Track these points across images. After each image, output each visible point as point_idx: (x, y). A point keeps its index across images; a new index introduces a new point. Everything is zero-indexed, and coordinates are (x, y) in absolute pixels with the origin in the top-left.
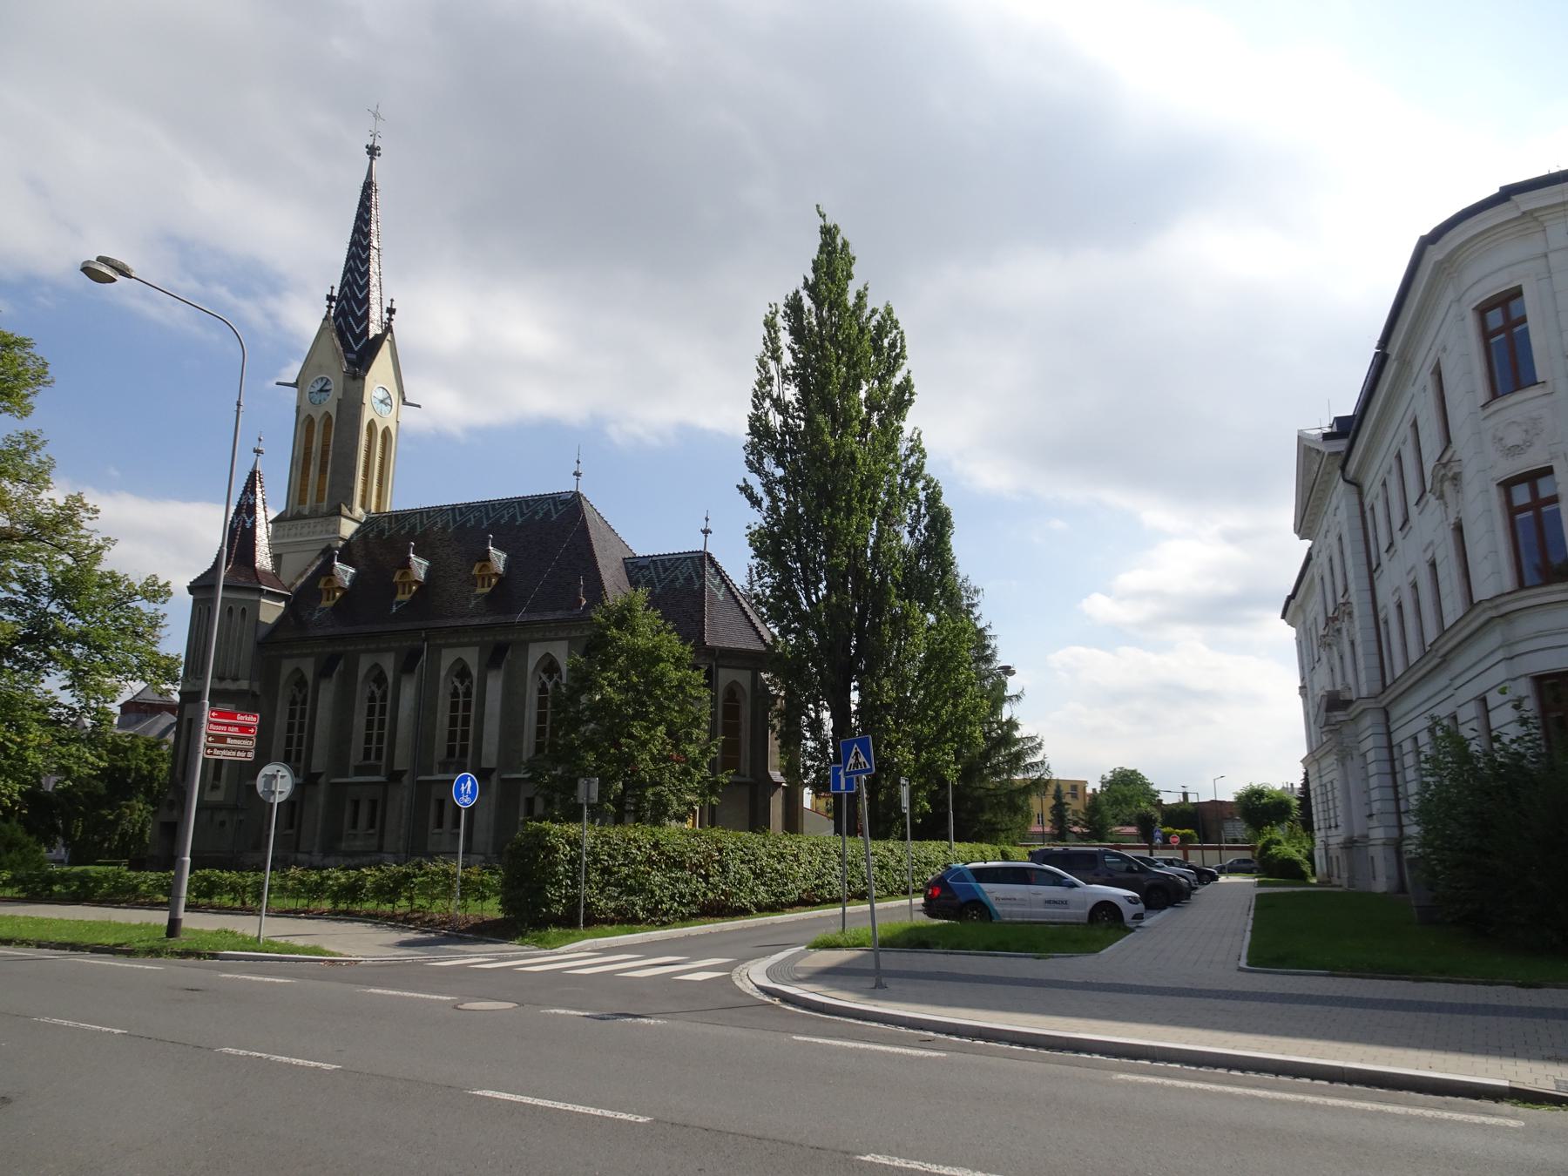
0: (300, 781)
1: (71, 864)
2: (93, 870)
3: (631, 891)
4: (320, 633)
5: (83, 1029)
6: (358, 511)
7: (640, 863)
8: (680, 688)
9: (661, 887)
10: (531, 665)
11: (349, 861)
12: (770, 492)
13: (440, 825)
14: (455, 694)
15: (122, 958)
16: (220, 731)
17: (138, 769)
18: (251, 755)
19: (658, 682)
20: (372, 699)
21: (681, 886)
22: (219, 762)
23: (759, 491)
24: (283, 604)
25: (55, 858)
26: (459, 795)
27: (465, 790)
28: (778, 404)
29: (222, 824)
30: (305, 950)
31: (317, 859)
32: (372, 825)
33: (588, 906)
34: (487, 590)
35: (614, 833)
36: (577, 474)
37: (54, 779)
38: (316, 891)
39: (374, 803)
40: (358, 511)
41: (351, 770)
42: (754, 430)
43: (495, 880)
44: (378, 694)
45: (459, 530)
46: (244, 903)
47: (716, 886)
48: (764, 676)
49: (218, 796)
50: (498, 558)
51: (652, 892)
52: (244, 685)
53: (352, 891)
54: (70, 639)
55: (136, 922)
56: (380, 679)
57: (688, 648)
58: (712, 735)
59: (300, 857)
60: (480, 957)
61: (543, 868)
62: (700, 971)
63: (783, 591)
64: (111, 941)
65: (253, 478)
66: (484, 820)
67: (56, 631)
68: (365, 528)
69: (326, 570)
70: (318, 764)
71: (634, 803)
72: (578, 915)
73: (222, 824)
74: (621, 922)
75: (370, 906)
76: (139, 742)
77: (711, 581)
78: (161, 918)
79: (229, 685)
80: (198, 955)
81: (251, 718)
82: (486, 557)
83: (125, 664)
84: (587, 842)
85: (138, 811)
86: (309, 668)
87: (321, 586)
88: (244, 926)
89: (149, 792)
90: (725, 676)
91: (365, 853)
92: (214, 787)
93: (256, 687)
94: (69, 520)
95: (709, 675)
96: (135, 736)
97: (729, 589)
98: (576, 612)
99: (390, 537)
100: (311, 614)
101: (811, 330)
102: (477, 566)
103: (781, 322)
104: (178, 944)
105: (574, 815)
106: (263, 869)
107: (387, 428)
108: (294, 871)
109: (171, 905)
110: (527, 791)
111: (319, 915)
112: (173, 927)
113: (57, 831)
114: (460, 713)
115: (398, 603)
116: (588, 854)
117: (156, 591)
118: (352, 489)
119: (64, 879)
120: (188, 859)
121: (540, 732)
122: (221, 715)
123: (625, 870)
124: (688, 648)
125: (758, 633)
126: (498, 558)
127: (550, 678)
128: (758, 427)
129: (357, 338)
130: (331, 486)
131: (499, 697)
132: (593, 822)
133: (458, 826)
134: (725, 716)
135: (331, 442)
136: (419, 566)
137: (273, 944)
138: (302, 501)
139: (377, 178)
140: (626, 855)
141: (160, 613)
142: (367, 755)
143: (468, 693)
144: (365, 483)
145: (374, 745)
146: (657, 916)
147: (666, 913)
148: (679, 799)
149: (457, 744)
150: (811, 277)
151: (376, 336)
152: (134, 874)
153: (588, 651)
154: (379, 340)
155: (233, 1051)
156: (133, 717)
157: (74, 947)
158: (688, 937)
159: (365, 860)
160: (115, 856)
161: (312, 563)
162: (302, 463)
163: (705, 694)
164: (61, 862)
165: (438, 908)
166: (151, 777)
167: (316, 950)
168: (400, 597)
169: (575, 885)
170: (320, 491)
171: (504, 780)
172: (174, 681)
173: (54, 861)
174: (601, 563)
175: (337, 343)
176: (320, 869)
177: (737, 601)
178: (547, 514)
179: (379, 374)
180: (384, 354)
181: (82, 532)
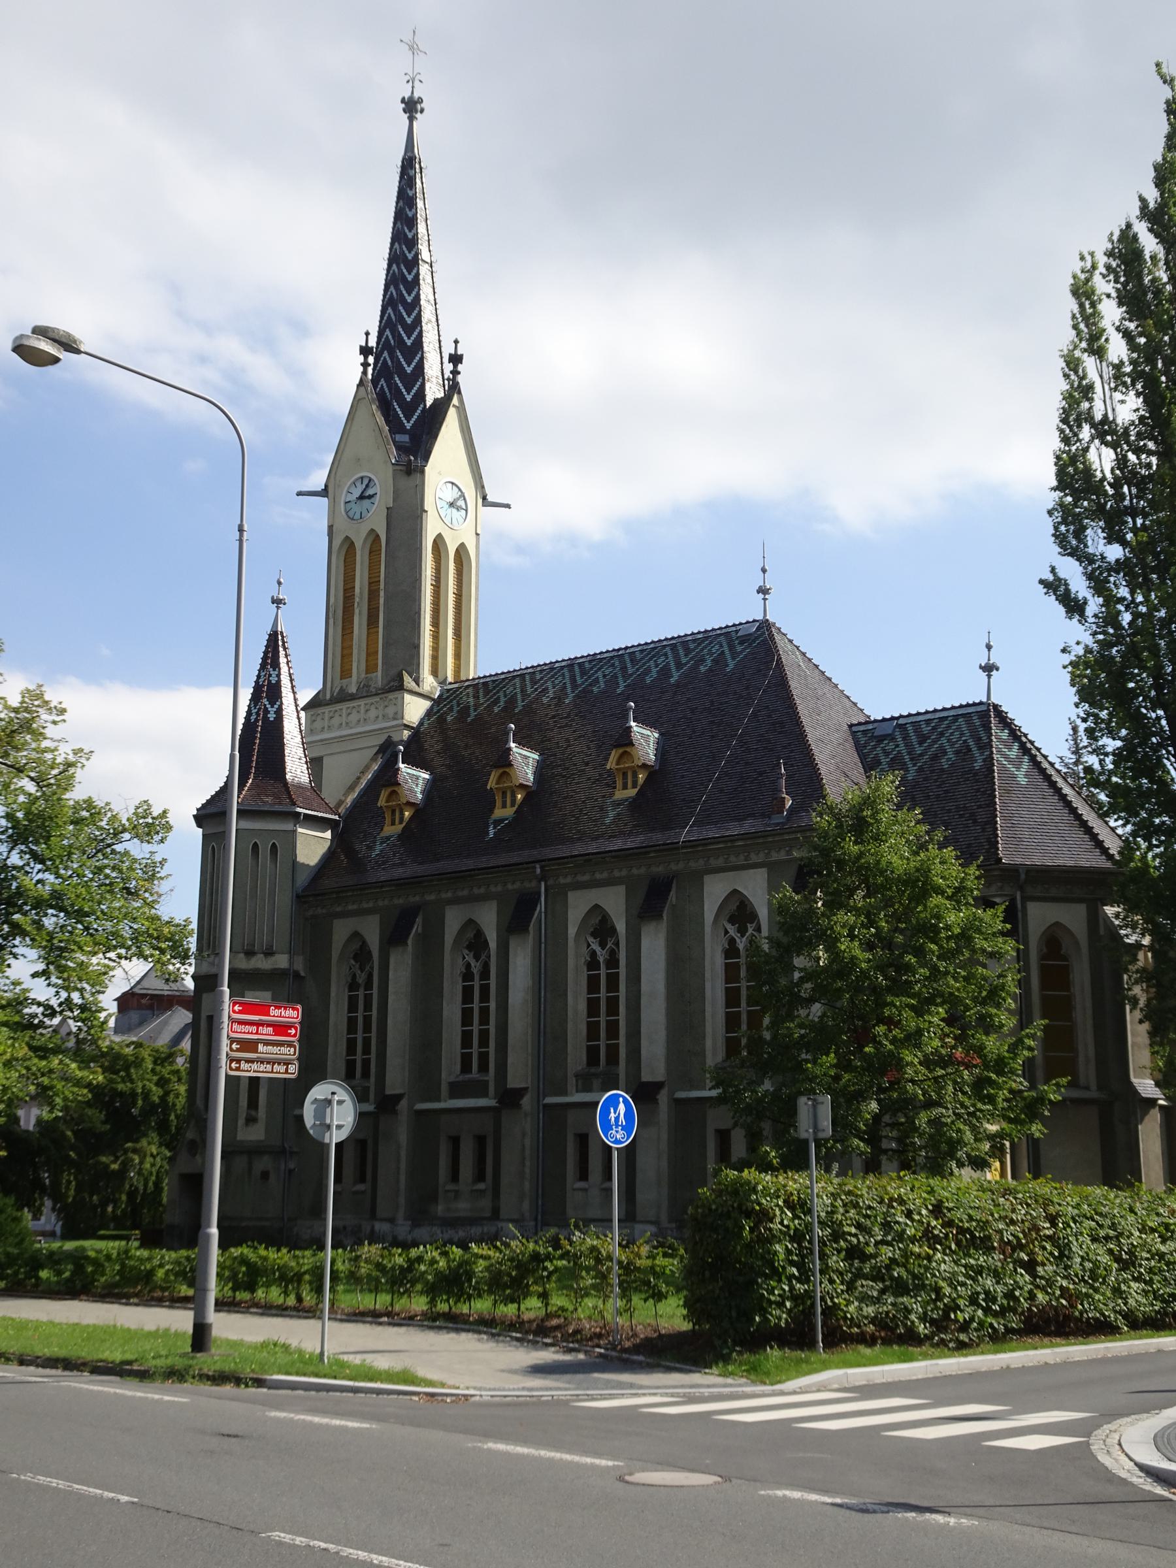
0: (369, 1107)
1: (67, 1235)
2: (92, 1246)
3: (900, 1288)
4: (383, 876)
5: (80, 1496)
6: (429, 683)
7: (913, 1240)
8: (965, 937)
9: (952, 1281)
10: (709, 914)
11: (450, 1233)
12: (1099, 585)
13: (583, 1175)
14: (593, 964)
15: (134, 1382)
16: (247, 1033)
17: (146, 1094)
18: (293, 1068)
19: (930, 931)
20: (468, 976)
21: (989, 1283)
22: (254, 1082)
23: (1079, 586)
24: (328, 834)
25: (40, 1227)
26: (607, 1127)
27: (617, 1120)
28: (1105, 430)
29: (265, 1175)
30: (390, 1377)
31: (403, 1230)
32: (480, 1176)
33: (829, 1312)
34: (632, 792)
35: (865, 1188)
36: (763, 591)
37: (35, 1112)
38: (400, 1281)
39: (481, 1140)
40: (429, 683)
41: (444, 1088)
42: (1064, 481)
43: (671, 1265)
44: (476, 967)
45: (585, 696)
46: (299, 1299)
47: (1050, 1283)
48: (1110, 910)
49: (254, 1134)
50: (646, 740)
51: (938, 1290)
52: (282, 961)
53: (454, 1283)
54: (40, 904)
55: (150, 1327)
56: (477, 944)
57: (973, 870)
58: (1024, 1018)
59: (381, 1227)
60: (658, 1394)
61: (749, 1247)
62: (1033, 1433)
63: (1139, 759)
64: (118, 1356)
65: (274, 642)
66: (652, 1166)
67: (19, 893)
68: (440, 706)
69: (387, 777)
70: (396, 1079)
71: (902, 1140)
72: (813, 1328)
73: (265, 1175)
74: (887, 1342)
75: (482, 1306)
76: (145, 1053)
77: (1003, 753)
78: (182, 1320)
79: (260, 963)
80: (238, 1381)
81: (290, 1013)
82: (625, 740)
83: (116, 934)
84: (821, 1205)
85: (150, 1156)
86: (372, 931)
87: (382, 802)
88: (300, 1334)
89: (163, 1127)
90: (1041, 915)
91: (473, 1221)
92: (251, 1120)
93: (299, 966)
94: (27, 726)
95: (1011, 915)
96: (139, 1045)
97: (1033, 759)
98: (776, 819)
99: (478, 718)
100: (370, 848)
101: (1158, 292)
102: (614, 755)
103: (1103, 286)
104: (208, 1362)
105: (795, 1160)
106: (322, 1247)
107: (462, 545)
108: (370, 1251)
109: (195, 1302)
110: (718, 1119)
111: (408, 1320)
112: (200, 1336)
113: (38, 1185)
114: (603, 994)
115: (497, 822)
116: (822, 1224)
117: (151, 826)
118: (416, 647)
119: (54, 1260)
120: (214, 1231)
121: (732, 1021)
122: (248, 1008)
123: (887, 1252)
124: (973, 870)
125: (1094, 837)
126: (646, 740)
127: (742, 931)
128: (1072, 475)
129: (409, 409)
130: (386, 645)
131: (661, 965)
132: (828, 1170)
133: (609, 1178)
134: (1044, 985)
135: (382, 577)
136: (525, 761)
137: (342, 1365)
138: (345, 673)
139: (422, 150)
140: (887, 1226)
141: (158, 858)
142: (466, 1067)
143: (613, 962)
144: (436, 636)
145: (475, 1050)
146: (947, 1333)
147: (965, 1327)
148: (974, 1129)
149: (602, 1044)
150: (1152, 195)
151: (436, 401)
152: (145, 1253)
153: (803, 878)
154: (441, 407)
155: (286, 1538)
156: (134, 1016)
157: (68, 1364)
158: (1007, 1371)
159: (476, 1231)
160: (122, 1226)
161: (367, 768)
162: (341, 614)
163: (1008, 947)
164: (51, 1235)
165: (588, 1311)
166: (165, 1105)
167: (406, 1377)
168: (499, 813)
169: (804, 1277)
170: (371, 654)
171: (678, 1102)
172: (184, 957)
173: (44, 1234)
174: (813, 735)
175: (380, 419)
176: (406, 1246)
177: (1053, 785)
178: (719, 660)
179: (445, 459)
180: (450, 428)
181: (45, 744)
